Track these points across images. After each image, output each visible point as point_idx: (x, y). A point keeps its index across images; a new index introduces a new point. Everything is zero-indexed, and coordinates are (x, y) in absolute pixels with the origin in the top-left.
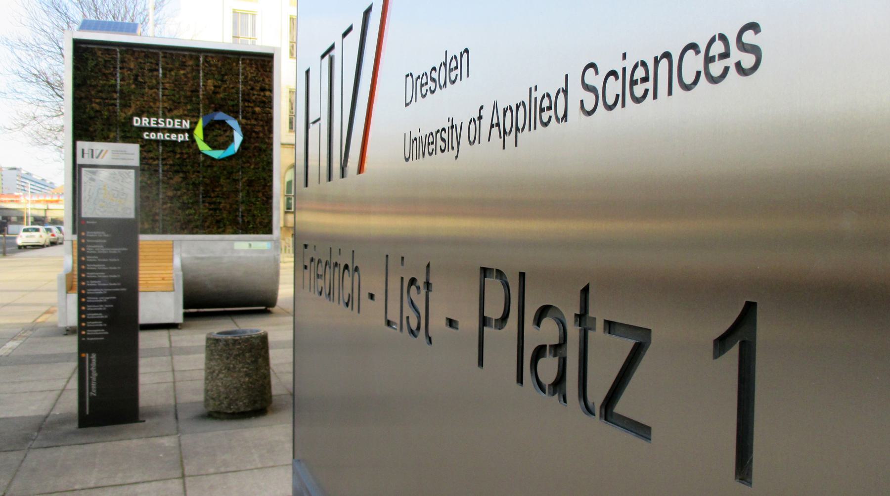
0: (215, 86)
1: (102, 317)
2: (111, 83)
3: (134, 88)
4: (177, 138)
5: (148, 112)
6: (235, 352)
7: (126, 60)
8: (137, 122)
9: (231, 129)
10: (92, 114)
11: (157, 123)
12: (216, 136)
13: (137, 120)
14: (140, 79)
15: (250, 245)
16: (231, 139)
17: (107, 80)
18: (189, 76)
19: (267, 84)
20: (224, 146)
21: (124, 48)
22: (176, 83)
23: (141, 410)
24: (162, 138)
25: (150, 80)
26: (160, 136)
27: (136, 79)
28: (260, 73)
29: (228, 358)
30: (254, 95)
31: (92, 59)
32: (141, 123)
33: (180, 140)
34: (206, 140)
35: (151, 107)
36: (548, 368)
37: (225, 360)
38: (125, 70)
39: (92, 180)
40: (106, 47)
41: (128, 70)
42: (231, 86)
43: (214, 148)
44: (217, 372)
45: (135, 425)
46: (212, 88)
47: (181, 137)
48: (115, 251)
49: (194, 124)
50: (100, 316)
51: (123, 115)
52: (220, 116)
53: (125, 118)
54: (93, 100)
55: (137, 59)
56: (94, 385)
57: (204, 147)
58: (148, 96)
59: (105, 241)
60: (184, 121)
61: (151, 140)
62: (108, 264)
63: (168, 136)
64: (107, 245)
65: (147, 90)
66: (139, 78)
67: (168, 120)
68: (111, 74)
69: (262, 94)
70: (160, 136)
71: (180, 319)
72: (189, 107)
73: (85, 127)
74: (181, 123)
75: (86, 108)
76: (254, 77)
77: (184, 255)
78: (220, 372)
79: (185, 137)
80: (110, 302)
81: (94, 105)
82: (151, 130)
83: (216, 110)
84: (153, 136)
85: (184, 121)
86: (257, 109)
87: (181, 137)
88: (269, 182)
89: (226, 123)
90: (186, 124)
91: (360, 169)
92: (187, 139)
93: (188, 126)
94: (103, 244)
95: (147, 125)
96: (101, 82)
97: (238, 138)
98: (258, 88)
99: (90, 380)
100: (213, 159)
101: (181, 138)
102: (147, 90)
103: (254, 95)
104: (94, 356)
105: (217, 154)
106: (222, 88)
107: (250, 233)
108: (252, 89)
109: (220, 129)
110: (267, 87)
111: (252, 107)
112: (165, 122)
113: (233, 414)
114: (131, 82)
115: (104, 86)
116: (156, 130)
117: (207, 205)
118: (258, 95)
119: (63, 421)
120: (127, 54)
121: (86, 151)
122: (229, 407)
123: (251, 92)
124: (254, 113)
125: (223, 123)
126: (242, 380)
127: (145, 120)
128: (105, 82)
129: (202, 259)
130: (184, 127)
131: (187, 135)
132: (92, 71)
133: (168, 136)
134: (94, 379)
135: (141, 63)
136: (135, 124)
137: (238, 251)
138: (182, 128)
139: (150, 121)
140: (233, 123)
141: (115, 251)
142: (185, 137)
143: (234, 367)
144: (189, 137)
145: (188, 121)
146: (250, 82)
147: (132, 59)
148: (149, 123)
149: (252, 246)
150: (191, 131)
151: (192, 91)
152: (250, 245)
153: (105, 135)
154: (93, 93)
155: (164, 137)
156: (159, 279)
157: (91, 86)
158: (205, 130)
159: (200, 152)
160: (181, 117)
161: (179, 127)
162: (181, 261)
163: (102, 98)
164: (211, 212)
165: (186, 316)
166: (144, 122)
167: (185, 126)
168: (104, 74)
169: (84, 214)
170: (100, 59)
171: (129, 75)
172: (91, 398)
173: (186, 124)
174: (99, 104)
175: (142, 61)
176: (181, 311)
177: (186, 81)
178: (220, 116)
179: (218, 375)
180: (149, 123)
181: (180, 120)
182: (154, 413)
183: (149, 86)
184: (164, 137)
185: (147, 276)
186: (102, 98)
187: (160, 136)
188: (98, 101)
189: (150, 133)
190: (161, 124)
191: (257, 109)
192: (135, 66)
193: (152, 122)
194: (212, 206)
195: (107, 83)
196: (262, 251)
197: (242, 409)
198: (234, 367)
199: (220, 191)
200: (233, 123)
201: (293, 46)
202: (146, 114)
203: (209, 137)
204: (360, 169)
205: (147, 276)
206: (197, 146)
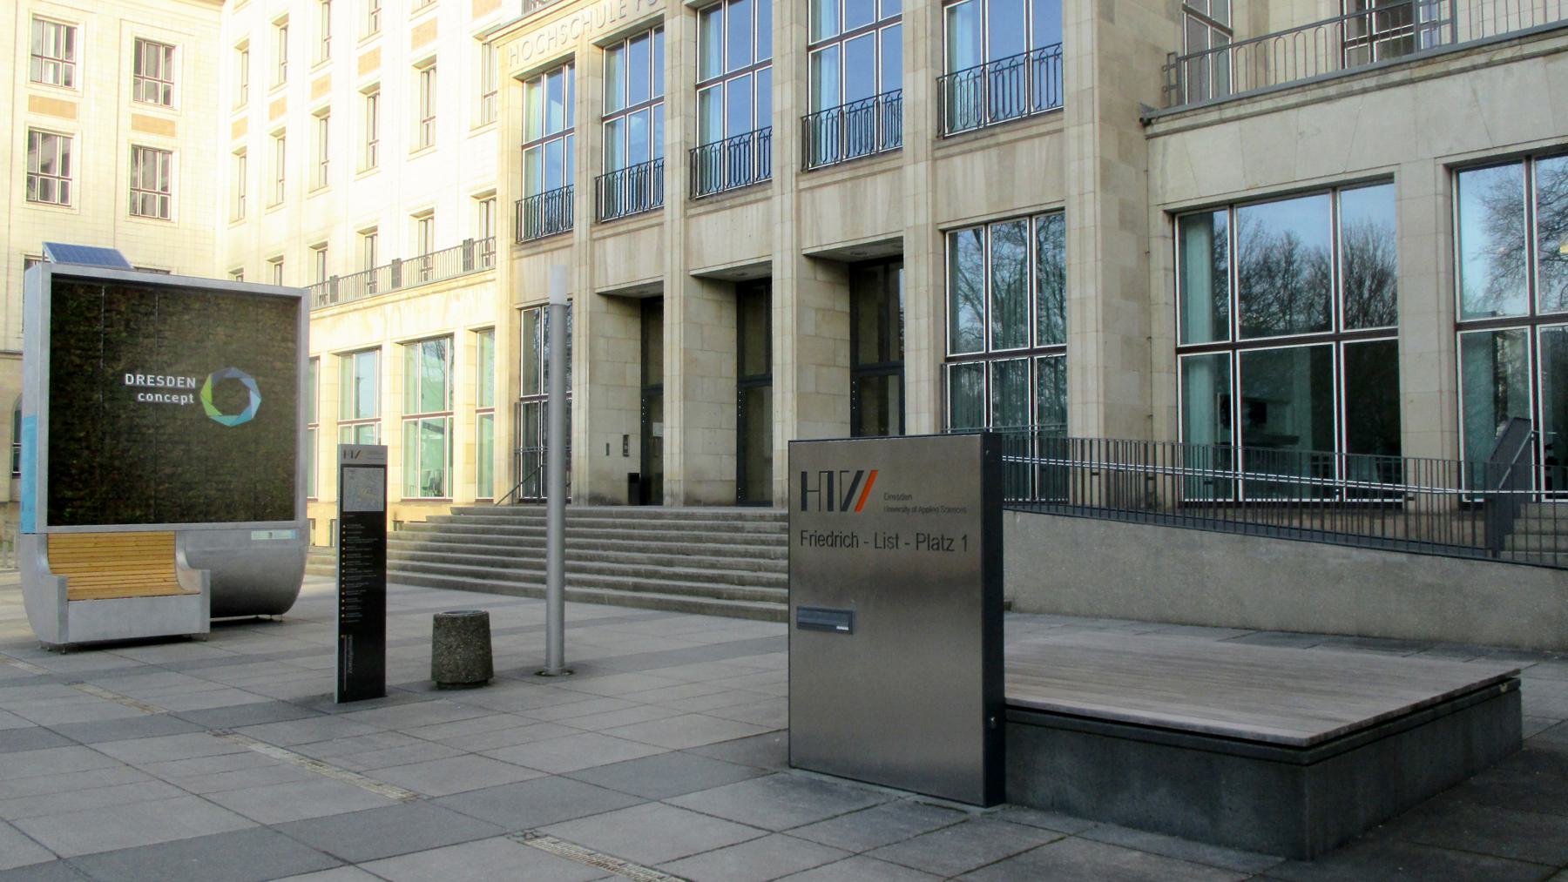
0: (226, 336)
1: (357, 601)
2: (95, 330)
3: (126, 337)
4: (180, 400)
5: (143, 367)
6: (472, 628)
7: (115, 300)
8: (129, 379)
9: (246, 389)
10: (72, 369)
11: (156, 382)
15: (271, 534)
16: (247, 401)
17: (90, 326)
19: (289, 333)
20: (237, 410)
21: (110, 285)
23: (387, 688)
24: (161, 400)
26: (159, 398)
27: (127, 325)
29: (465, 634)
30: (273, 346)
31: (72, 299)
32: (135, 381)
33: (183, 402)
34: (215, 403)
35: (146, 361)
36: (935, 547)
37: (463, 636)
38: (114, 313)
39: (352, 478)
40: (88, 283)
41: (117, 314)
43: (224, 412)
44: (454, 647)
45: (383, 699)
46: (223, 337)
47: (184, 399)
48: (368, 541)
49: (201, 382)
50: (356, 600)
51: (111, 371)
52: (234, 372)
53: (113, 375)
54: (72, 351)
55: (129, 299)
56: (350, 665)
57: (212, 412)
59: (360, 532)
60: (189, 379)
61: (146, 403)
62: (363, 553)
63: (168, 398)
64: (361, 536)
65: (141, 339)
66: (132, 323)
67: (168, 378)
68: (95, 318)
69: (283, 345)
70: (159, 398)
71: (207, 630)
73: (61, 385)
74: (185, 381)
76: (274, 324)
77: (189, 549)
78: (458, 646)
79: (189, 400)
80: (362, 588)
81: (73, 358)
82: (146, 390)
83: (228, 366)
84: (150, 397)
85: (189, 379)
86: (278, 365)
87: (184, 399)
88: (291, 455)
89: (241, 382)
90: (191, 383)
91: (858, 508)
92: (192, 401)
93: (193, 385)
94: (358, 535)
95: (143, 383)
96: (82, 328)
97: (255, 401)
98: (279, 338)
99: (348, 659)
100: (222, 426)
101: (184, 400)
102: (141, 339)
103: (273, 346)
104: (351, 638)
105: (229, 421)
107: (267, 520)
108: (272, 339)
110: (290, 336)
112: (165, 380)
113: (470, 684)
114: (122, 328)
115: (85, 333)
116: (154, 390)
117: (214, 484)
118: (279, 347)
119: (325, 697)
120: (117, 293)
121: (347, 452)
122: (467, 675)
124: (273, 368)
125: (235, 382)
126: (478, 653)
127: (140, 378)
128: (87, 328)
129: (211, 553)
130: (188, 386)
131: (191, 396)
132: (73, 314)
133: (168, 398)
134: (351, 657)
135: (133, 305)
136: (127, 382)
137: (257, 542)
139: (146, 378)
140: (249, 381)
141: (368, 541)
142: (189, 400)
143: (471, 642)
144: (193, 400)
145: (194, 379)
146: (268, 331)
147: (123, 300)
148: (145, 381)
149: (274, 534)
150: (196, 392)
152: (271, 534)
154: (72, 341)
155: (163, 399)
156: (161, 580)
157: (70, 332)
159: (207, 419)
160: (185, 374)
161: (183, 386)
162: (187, 557)
163: (83, 349)
164: (220, 493)
165: (213, 625)
166: (138, 380)
168: (87, 319)
170: (82, 299)
171: (119, 319)
172: (348, 675)
173: (191, 383)
174: (80, 356)
175: (136, 303)
176: (208, 620)
178: (234, 372)
179: (456, 649)
180: (145, 381)
182: (398, 689)
183: (144, 334)
185: (144, 577)
186: (83, 349)
187: (158, 397)
188: (78, 352)
189: (146, 393)
190: (161, 383)
191: (278, 365)
192: (126, 309)
193: (149, 380)
194: (220, 486)
195: (91, 329)
196: (286, 542)
197: (478, 679)
198: (471, 642)
199: (232, 466)
200: (249, 381)
202: (140, 370)
204: (858, 508)
205: (144, 577)
206: (203, 410)
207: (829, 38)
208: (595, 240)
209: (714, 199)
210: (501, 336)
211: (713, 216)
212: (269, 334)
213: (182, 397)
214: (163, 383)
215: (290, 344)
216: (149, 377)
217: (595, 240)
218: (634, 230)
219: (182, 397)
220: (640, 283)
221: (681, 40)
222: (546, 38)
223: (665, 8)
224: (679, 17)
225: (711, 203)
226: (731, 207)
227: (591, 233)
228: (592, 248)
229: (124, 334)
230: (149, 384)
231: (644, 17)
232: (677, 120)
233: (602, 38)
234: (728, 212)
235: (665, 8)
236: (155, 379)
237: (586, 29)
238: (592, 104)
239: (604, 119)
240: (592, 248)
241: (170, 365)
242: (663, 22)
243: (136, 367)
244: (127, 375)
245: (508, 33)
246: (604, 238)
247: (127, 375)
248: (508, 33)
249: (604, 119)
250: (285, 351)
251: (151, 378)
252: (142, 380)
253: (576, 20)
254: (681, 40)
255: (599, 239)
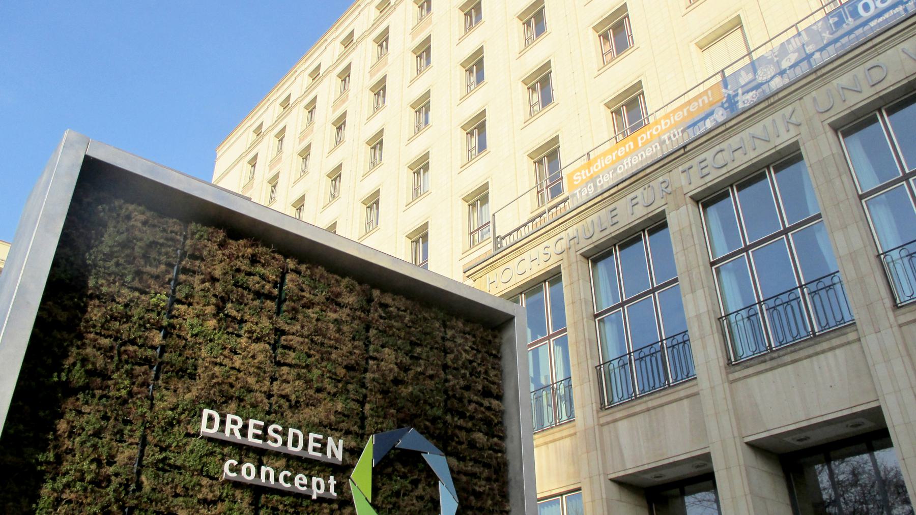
0: (400, 366)
5: (241, 400)
9: (432, 479)
11: (264, 437)
12: (397, 494)
13: (211, 419)
14: (230, 309)
18: (345, 328)
22: (317, 339)
25: (255, 319)
28: (480, 356)
30: (470, 401)
42: (430, 372)
49: (354, 453)
58: (245, 357)
60: (330, 441)
63: (286, 479)
65: (243, 341)
72: (340, 406)
75: (66, 356)
79: (327, 489)
82: (243, 451)
83: (402, 423)
92: (333, 493)
95: (238, 434)
102: (243, 341)
103: (470, 401)
106: (411, 374)
109: (404, 477)
110: (494, 388)
111: (469, 431)
112: (284, 434)
114: (210, 309)
116: (260, 455)
123: (466, 394)
124: (472, 444)
125: (413, 459)
127: (234, 422)
131: (332, 481)
135: (238, 270)
138: (323, 460)
139: (245, 427)
140: (437, 462)
142: (327, 489)
145: (341, 442)
148: (244, 431)
150: (342, 470)
151: (349, 368)
153: (104, 453)
155: (277, 480)
158: (377, 472)
160: (326, 427)
167: (333, 455)
169: (711, 481)
173: (336, 449)
177: (337, 340)
178: (411, 439)
180: (244, 431)
181: (320, 437)
184: (277, 480)
190: (275, 431)
193: (251, 431)
201: (281, 149)
202: (233, 405)
203: (380, 498)
207: (876, 187)
208: (602, 425)
209: (767, 357)
210: (586, 494)
211: (769, 374)
212: (464, 376)
213: (315, 480)
214: (280, 439)
215: (495, 403)
216: (252, 422)
217: (602, 425)
218: (654, 408)
219: (315, 480)
220: (671, 460)
221: (690, 225)
222: (528, 261)
223: (667, 204)
224: (685, 207)
225: (765, 361)
226: (794, 361)
227: (599, 418)
228: (601, 433)
229: (212, 323)
230: (251, 439)
231: (640, 218)
232: (700, 292)
233: (592, 246)
234: (790, 367)
235: (667, 204)
236: (265, 429)
237: (571, 244)
238: (586, 302)
239: (596, 316)
240: (601, 433)
241: (295, 406)
242: (666, 218)
243: (228, 399)
244: (206, 412)
245: (487, 266)
246: (615, 421)
247: (206, 412)
248: (487, 266)
249: (596, 316)
250: (488, 413)
251: (256, 427)
252: (236, 429)
253: (561, 239)
254: (690, 225)
255: (608, 423)
